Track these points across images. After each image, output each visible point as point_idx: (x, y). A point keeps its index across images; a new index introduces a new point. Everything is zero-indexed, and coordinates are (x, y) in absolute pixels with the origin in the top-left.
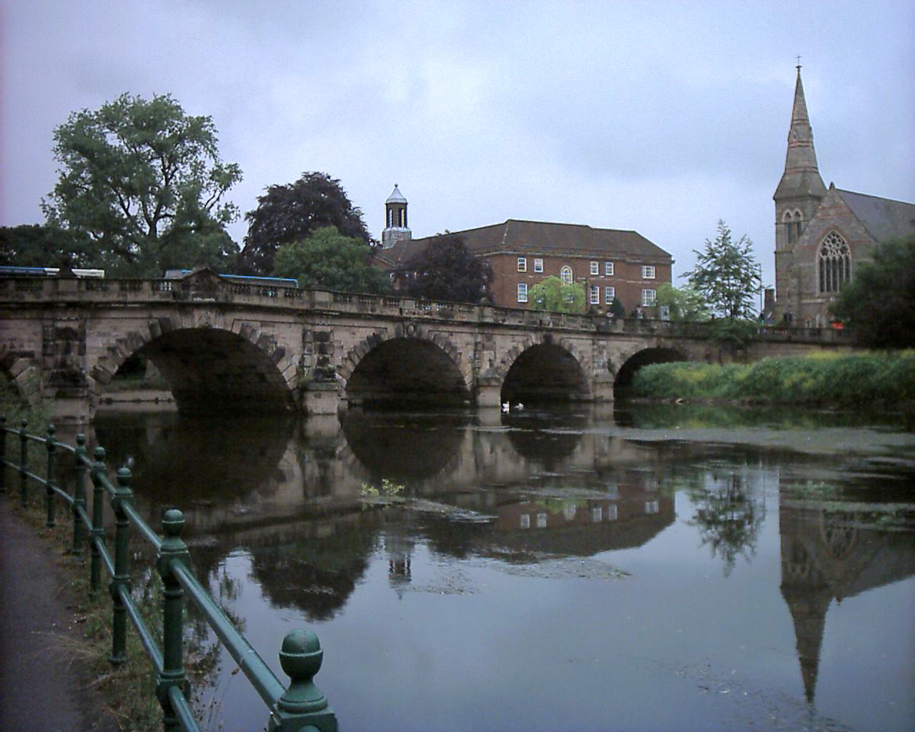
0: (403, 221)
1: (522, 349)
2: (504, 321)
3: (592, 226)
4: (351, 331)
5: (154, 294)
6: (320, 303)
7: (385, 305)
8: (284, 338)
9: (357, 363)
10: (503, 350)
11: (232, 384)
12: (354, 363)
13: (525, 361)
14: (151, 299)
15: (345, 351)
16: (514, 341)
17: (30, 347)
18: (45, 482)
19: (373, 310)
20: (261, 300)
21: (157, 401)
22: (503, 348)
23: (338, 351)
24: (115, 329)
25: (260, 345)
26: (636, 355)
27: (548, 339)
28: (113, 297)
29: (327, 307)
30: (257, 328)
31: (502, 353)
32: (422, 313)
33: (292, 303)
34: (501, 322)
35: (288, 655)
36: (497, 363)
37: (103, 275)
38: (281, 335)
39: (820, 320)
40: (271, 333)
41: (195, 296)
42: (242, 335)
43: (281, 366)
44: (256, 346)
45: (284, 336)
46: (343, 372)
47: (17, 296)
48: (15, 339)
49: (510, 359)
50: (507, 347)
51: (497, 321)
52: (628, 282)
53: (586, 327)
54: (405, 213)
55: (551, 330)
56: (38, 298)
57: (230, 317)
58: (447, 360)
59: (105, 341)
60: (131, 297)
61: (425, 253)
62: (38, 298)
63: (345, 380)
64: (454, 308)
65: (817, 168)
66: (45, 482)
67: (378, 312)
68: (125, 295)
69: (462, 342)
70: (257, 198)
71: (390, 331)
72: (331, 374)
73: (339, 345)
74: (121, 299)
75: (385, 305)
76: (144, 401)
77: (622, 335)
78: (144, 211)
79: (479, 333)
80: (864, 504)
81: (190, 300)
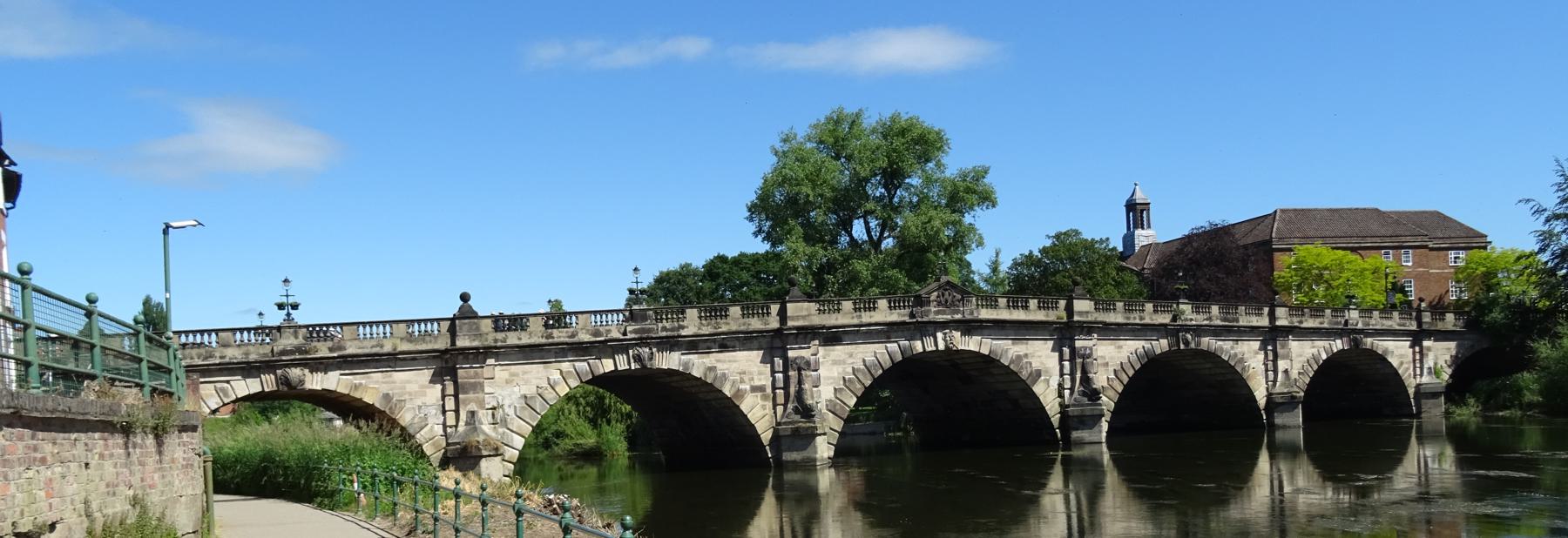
0: (1145, 223)
1: (1324, 357)
2: (1301, 322)
3: (1383, 208)
4: (1117, 345)
6: (1080, 313)
7: (1156, 311)
8: (1040, 357)
9: (1125, 383)
10: (1300, 359)
12: (1122, 382)
13: (1327, 371)
15: (1111, 369)
16: (1314, 347)
17: (760, 380)
19: (1141, 319)
20: (1011, 314)
22: (1301, 356)
23: (1103, 369)
24: (851, 356)
25: (1012, 367)
27: (1356, 344)
29: (1087, 317)
30: (1008, 350)
31: (1300, 362)
32: (1199, 319)
33: (1047, 316)
34: (1296, 324)
35: (1503, 473)
36: (1294, 374)
38: (1345, 261)
39: (1526, 427)
40: (1025, 352)
41: (937, 313)
42: (991, 355)
43: (1038, 389)
44: (1008, 367)
45: (1039, 354)
47: (744, 324)
48: (744, 373)
49: (1310, 369)
50: (1302, 357)
51: (1293, 323)
52: (1431, 271)
53: (1404, 325)
55: (1361, 331)
56: (765, 324)
58: (1232, 380)
59: (840, 370)
61: (1179, 252)
62: (765, 324)
64: (1239, 311)
65: (149, 373)
67: (1147, 321)
68: (860, 317)
69: (1249, 356)
70: (276, 304)
71: (1162, 345)
73: (1103, 361)
74: (856, 321)
75: (1156, 311)
78: (869, 227)
79: (1270, 339)
81: (932, 317)
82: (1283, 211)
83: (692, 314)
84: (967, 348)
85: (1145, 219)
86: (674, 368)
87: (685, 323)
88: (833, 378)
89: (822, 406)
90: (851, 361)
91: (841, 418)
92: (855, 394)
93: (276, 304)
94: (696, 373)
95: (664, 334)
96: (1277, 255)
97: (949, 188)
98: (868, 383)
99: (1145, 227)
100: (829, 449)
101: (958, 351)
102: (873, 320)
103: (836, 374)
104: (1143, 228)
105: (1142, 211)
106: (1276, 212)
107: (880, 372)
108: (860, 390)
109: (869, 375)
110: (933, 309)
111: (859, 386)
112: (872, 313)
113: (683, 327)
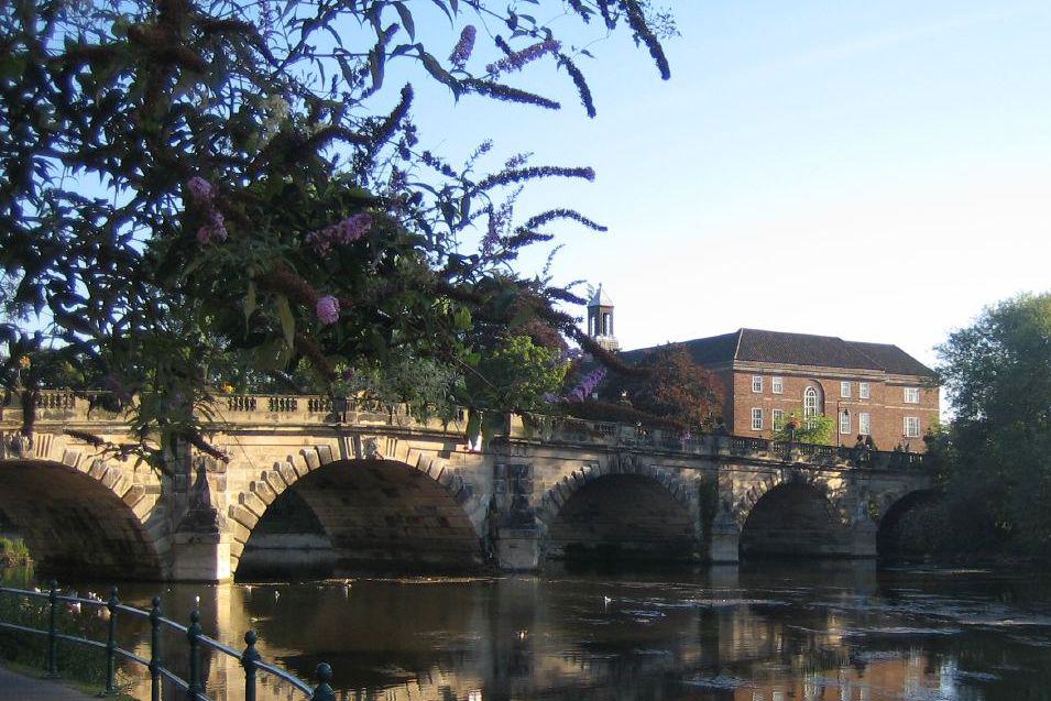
0: (608, 329)
5: (311, 415)
9: (561, 505)
11: (406, 529)
14: (308, 422)
18: (187, 686)
21: (306, 549)
24: (263, 459)
26: (904, 498)
28: (261, 419)
37: (322, 154)
41: (361, 418)
46: (545, 516)
54: (611, 319)
57: (402, 445)
60: (282, 418)
63: (546, 526)
66: (187, 686)
68: (275, 417)
70: (409, 85)
72: (529, 517)
74: (270, 421)
76: (262, 548)
77: (884, 472)
80: (219, 546)
82: (745, 330)
83: (82, 404)
84: (392, 458)
85: (608, 324)
86: (56, 460)
87: (73, 411)
88: (242, 483)
89: (224, 513)
90: (262, 464)
91: (246, 526)
92: (265, 503)
93: (409, 85)
94: (84, 468)
95: (47, 421)
96: (736, 374)
97: (206, 367)
98: (280, 490)
99: (608, 333)
100: (232, 561)
101: (383, 461)
102: (290, 421)
103: (244, 479)
104: (605, 334)
105: (605, 314)
106: (740, 330)
107: (296, 478)
108: (270, 497)
109: (281, 481)
110: (358, 414)
111: (270, 493)
112: (290, 413)
113: (71, 415)
